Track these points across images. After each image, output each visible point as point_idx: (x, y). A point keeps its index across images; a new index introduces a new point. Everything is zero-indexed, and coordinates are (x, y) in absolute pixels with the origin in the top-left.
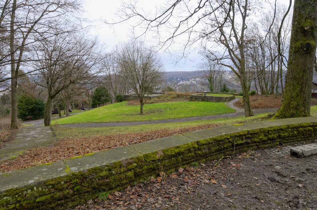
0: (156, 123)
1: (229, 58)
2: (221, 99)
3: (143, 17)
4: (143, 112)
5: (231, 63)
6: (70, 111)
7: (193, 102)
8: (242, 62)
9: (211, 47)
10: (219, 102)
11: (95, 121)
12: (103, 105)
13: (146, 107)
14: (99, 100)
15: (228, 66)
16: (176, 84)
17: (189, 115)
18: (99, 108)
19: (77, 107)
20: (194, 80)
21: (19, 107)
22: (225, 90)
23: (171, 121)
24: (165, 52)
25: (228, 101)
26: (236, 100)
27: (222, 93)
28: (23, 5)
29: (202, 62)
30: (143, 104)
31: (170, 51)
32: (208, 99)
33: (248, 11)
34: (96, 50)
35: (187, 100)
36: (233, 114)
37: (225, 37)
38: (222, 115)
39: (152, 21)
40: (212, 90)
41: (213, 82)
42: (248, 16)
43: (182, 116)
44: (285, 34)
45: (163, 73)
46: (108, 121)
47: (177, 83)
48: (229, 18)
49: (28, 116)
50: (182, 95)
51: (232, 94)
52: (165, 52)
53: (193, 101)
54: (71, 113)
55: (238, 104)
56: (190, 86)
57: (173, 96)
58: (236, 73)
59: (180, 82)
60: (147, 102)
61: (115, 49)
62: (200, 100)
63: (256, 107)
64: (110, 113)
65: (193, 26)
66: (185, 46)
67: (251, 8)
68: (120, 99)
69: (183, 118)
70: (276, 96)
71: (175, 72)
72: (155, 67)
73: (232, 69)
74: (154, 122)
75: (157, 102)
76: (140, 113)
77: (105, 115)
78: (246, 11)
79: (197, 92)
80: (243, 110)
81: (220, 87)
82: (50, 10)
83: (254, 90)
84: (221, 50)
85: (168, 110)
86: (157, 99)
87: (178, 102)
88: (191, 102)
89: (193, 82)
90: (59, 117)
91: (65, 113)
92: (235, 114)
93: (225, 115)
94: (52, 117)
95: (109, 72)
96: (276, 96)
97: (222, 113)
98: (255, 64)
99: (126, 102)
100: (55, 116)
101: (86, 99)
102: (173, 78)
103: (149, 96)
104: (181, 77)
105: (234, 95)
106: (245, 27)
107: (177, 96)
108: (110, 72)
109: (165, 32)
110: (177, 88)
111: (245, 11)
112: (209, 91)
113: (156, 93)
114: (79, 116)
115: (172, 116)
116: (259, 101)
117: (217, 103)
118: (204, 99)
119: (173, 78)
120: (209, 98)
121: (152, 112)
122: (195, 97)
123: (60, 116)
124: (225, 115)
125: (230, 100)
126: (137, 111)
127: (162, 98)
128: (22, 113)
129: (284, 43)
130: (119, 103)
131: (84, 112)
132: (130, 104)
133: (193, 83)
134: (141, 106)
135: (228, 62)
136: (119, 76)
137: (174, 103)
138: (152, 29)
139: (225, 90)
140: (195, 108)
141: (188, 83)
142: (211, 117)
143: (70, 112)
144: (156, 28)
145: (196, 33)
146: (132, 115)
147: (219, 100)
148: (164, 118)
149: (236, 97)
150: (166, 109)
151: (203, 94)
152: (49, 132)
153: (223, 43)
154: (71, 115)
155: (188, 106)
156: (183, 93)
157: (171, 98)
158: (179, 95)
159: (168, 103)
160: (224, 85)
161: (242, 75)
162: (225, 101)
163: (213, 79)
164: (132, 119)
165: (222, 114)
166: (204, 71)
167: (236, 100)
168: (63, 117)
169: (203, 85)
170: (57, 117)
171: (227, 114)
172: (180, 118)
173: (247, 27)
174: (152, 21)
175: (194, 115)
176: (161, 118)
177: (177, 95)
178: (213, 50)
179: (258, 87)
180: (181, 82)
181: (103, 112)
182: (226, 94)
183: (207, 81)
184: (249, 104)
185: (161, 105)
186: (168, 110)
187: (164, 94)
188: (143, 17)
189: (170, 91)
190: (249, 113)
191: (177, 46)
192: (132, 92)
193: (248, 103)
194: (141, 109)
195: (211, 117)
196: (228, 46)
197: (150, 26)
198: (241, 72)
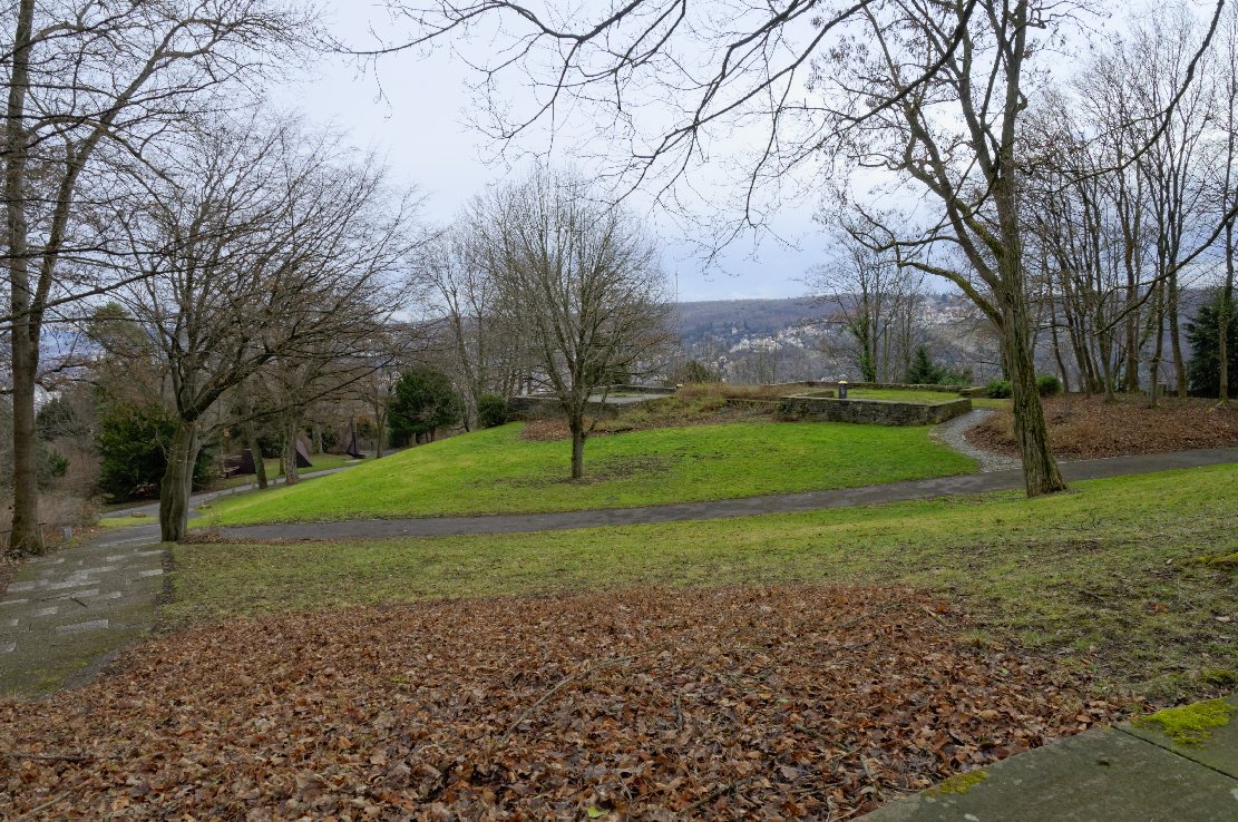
0: (637, 522)
1: (950, 239)
2: (914, 412)
3: (534, 19)
4: (584, 469)
5: (959, 262)
6: (302, 462)
7: (794, 427)
8: (1007, 250)
9: (871, 192)
10: (901, 425)
11: (382, 511)
12: (429, 435)
13: (598, 449)
14: (417, 413)
15: (945, 274)
16: (722, 350)
17: (779, 487)
18: (418, 448)
19: (330, 444)
20: (794, 332)
21: (107, 449)
22: (924, 373)
23: (699, 514)
24: (658, 205)
25: (943, 421)
26: (978, 416)
27: (915, 388)
28: (65, 31)
29: (827, 259)
30: (583, 436)
31: (682, 204)
32: (855, 413)
33: (1031, 33)
34: (376, 212)
35: (767, 417)
36: (968, 482)
37: (930, 146)
38: (922, 485)
39: (581, 40)
40: (870, 376)
41: (875, 340)
42: (1028, 55)
43: (746, 487)
44: (1189, 134)
45: (666, 309)
46: (438, 510)
47: (730, 348)
48: (948, 63)
49: (140, 482)
50: (746, 396)
51: (957, 391)
52: (658, 205)
53: (792, 420)
54: (309, 468)
55: (986, 435)
56: (777, 355)
57: (708, 403)
58: (982, 303)
59: (738, 342)
60: (601, 425)
61: (471, 212)
62: (824, 415)
63: (1069, 450)
64: (448, 475)
65: (793, 67)
66: (758, 191)
67: (1045, 16)
68: (495, 416)
69: (754, 496)
70: (1155, 399)
71: (721, 303)
72: (634, 284)
73: (964, 285)
74: (626, 516)
75: (644, 425)
76: (570, 475)
77: (427, 485)
78: (1024, 33)
79: (811, 384)
80: (1014, 463)
81: (903, 362)
82: (178, 48)
83: (1054, 373)
84: (917, 208)
85: (688, 460)
86: (643, 414)
87: (730, 426)
88: (786, 427)
89: (790, 340)
90: (257, 485)
91: (282, 472)
92: (978, 480)
93: (932, 484)
94: (194, 502)
95: (453, 305)
96: (1155, 399)
97: (918, 475)
98: (1052, 263)
99: (519, 426)
100: (245, 484)
101: (368, 412)
102: (710, 328)
103: (608, 400)
104: (743, 323)
105: (965, 394)
106: (1019, 101)
107: (723, 400)
108: (456, 304)
109: (656, 105)
110: (729, 367)
111: (1020, 33)
112: (859, 378)
113: (642, 390)
114: (332, 485)
115: (705, 491)
116: (1081, 423)
117: (894, 428)
118: (840, 413)
119: (710, 328)
120: (859, 408)
121: (620, 469)
122: (803, 403)
123: (263, 484)
124: (932, 484)
125: (951, 418)
126: (560, 468)
127: (664, 408)
128: (118, 471)
129: (1181, 173)
130: (490, 432)
131: (360, 463)
132: (534, 437)
133: (792, 346)
134: (574, 446)
135: (946, 254)
136: (492, 322)
137: (714, 428)
138: (590, 89)
139: (924, 374)
140: (802, 452)
141: (771, 344)
142: (873, 496)
143: (299, 466)
144: (605, 89)
145: (804, 116)
146: (535, 483)
147: (904, 416)
148: (667, 499)
149: (975, 402)
150: (678, 458)
151: (836, 393)
152: (151, 573)
153: (921, 175)
154: (306, 480)
155: (771, 442)
156: (753, 389)
157: (701, 411)
158: (734, 397)
159: (688, 430)
160: (921, 354)
161: (1010, 312)
162: (930, 421)
163: (875, 328)
164: (538, 500)
165: (923, 479)
166: (837, 299)
167: (978, 416)
168: (276, 487)
169: (832, 352)
170: (250, 487)
171: (940, 481)
172: (737, 497)
173: (1025, 101)
174: (581, 40)
175: (799, 486)
176: (656, 499)
177: (724, 394)
178: (875, 206)
179: (1072, 362)
180: (745, 343)
181: (420, 470)
182: (932, 389)
183: (853, 339)
184: (1043, 440)
185: (659, 440)
186: (688, 460)
187: (672, 391)
188: (534, 19)
189: (699, 381)
190: (1044, 480)
191: (711, 181)
192: (540, 389)
193: (1040, 435)
194: (576, 459)
195: (873, 496)
196: (945, 189)
197: (574, 77)
198: (1003, 297)
